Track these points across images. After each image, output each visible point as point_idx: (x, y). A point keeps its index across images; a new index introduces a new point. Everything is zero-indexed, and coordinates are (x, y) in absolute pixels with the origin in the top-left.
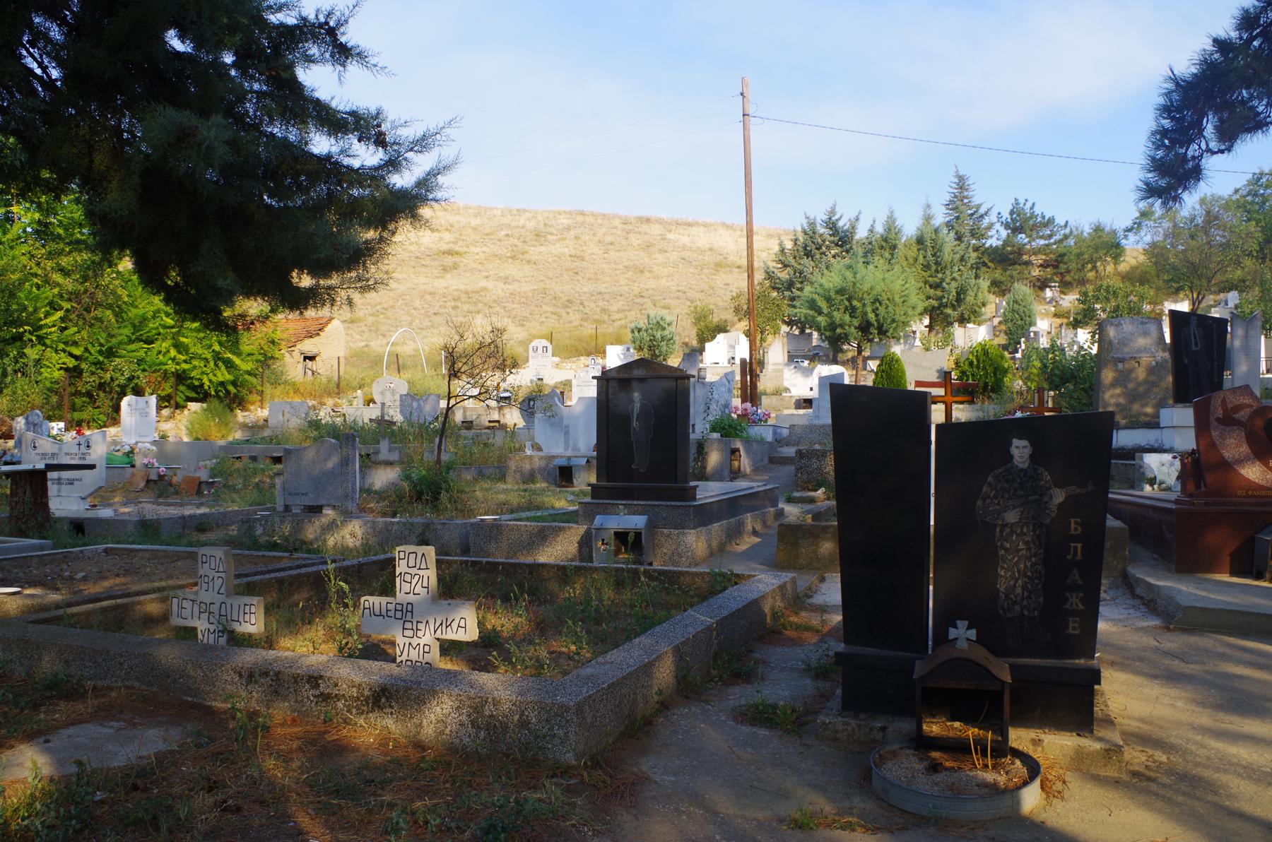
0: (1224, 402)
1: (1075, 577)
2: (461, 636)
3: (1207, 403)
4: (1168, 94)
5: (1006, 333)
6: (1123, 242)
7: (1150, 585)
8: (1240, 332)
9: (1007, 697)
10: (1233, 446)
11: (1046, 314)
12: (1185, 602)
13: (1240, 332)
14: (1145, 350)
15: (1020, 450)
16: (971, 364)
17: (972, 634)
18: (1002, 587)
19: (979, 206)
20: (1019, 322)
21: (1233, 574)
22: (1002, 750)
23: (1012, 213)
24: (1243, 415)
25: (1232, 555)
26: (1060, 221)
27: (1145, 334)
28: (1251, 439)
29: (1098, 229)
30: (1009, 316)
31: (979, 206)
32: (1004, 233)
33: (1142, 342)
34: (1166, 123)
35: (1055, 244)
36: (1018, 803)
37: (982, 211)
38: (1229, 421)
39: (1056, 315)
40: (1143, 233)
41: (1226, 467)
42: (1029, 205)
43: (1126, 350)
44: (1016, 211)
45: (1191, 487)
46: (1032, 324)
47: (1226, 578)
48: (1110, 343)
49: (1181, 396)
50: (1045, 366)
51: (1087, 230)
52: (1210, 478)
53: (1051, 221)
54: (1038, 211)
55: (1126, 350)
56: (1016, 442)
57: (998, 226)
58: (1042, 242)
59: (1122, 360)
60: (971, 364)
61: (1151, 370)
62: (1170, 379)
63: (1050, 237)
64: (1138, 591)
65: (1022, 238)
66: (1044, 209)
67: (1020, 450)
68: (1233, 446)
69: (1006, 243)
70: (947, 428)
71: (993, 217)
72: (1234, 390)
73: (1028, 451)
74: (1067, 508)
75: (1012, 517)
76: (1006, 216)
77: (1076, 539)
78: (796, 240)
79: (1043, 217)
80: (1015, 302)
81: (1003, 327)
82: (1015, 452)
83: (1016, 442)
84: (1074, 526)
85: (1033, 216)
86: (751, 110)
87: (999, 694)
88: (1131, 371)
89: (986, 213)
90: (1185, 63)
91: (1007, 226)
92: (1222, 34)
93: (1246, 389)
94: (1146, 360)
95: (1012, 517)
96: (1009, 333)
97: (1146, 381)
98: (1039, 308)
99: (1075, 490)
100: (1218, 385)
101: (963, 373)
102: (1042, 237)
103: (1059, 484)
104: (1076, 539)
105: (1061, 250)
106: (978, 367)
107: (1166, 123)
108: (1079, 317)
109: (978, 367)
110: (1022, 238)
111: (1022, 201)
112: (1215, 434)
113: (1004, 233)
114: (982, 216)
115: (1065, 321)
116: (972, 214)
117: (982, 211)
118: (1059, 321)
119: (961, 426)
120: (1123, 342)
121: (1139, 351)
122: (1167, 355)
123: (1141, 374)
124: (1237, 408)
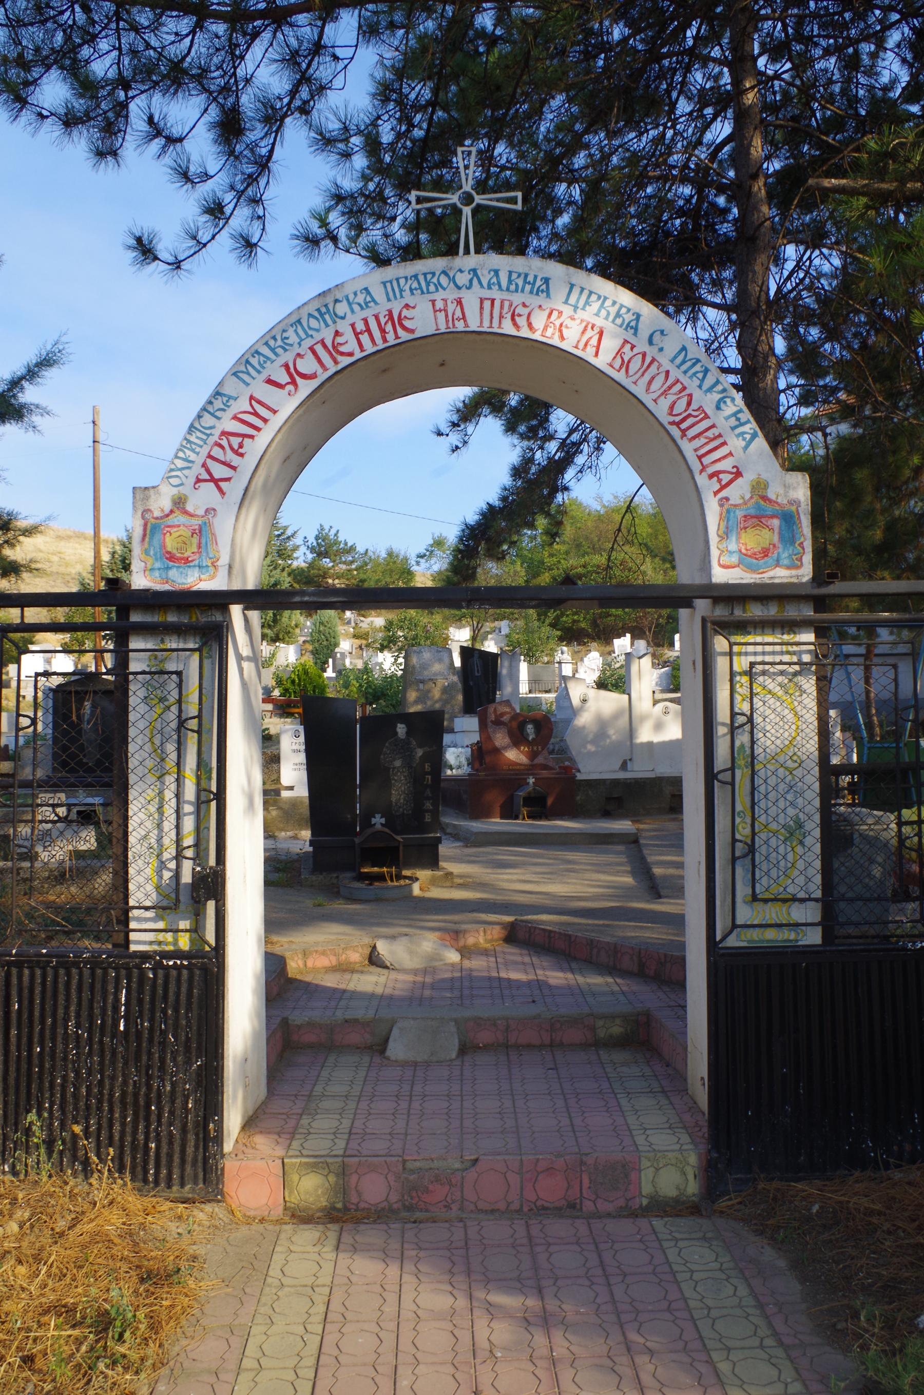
0: (495, 710)
1: (428, 792)
2: (83, 847)
3: (485, 711)
4: (463, 531)
5: (312, 652)
6: (415, 568)
7: (455, 826)
8: (506, 664)
9: (401, 848)
10: (500, 739)
11: (347, 635)
12: (475, 830)
13: (506, 664)
14: (440, 674)
15: (401, 729)
16: (293, 682)
17: (383, 821)
18: (394, 799)
19: (286, 528)
20: (325, 643)
21: (502, 818)
22: (399, 877)
23: (317, 538)
24: (506, 718)
25: (502, 807)
26: (360, 549)
27: (440, 660)
28: (511, 734)
29: (390, 554)
30: (316, 636)
31: (286, 528)
32: (310, 556)
33: (437, 667)
34: (461, 547)
35: (356, 569)
36: (411, 891)
37: (289, 532)
38: (498, 723)
39: (355, 636)
40: (432, 562)
41: (497, 751)
42: (333, 532)
43: (426, 673)
44: (321, 536)
45: (477, 765)
46: (336, 645)
47: (498, 820)
48: (414, 667)
49: (469, 709)
50: (361, 686)
51: (383, 554)
52: (488, 759)
53: (352, 549)
54: (341, 538)
55: (426, 673)
56: (399, 725)
57: (303, 549)
58: (344, 567)
59: (422, 682)
60: (293, 682)
61: (445, 690)
62: (460, 697)
63: (352, 562)
64: (448, 831)
65: (326, 562)
66: (348, 536)
67: (401, 729)
68: (500, 739)
69: (311, 565)
70: (364, 718)
71: (298, 541)
72: (501, 703)
73: (405, 730)
74: (424, 759)
75: (398, 763)
76: (312, 540)
77: (428, 773)
78: (114, 553)
79: (346, 544)
80: (321, 623)
81: (310, 648)
82: (399, 730)
83: (399, 725)
84: (427, 767)
85: (336, 542)
86: (101, 437)
87: (397, 848)
88: (429, 691)
89: (293, 536)
90: (472, 518)
91: (312, 550)
92: (491, 502)
93: (507, 703)
94: (442, 682)
95: (398, 763)
96: (315, 653)
97: (440, 700)
98: (341, 629)
99: (427, 749)
100: (493, 700)
101: (286, 690)
102: (344, 563)
103: (420, 746)
104: (428, 773)
105: (362, 576)
106: (299, 685)
107: (461, 547)
108: (385, 643)
109: (299, 685)
110: (326, 562)
111: (327, 528)
112: (490, 730)
113: (310, 556)
114: (288, 538)
115: (364, 642)
116: (279, 536)
117: (289, 532)
118: (358, 642)
119: (370, 717)
120: (424, 667)
121: (435, 674)
122: (455, 678)
123: (436, 693)
124: (502, 714)
